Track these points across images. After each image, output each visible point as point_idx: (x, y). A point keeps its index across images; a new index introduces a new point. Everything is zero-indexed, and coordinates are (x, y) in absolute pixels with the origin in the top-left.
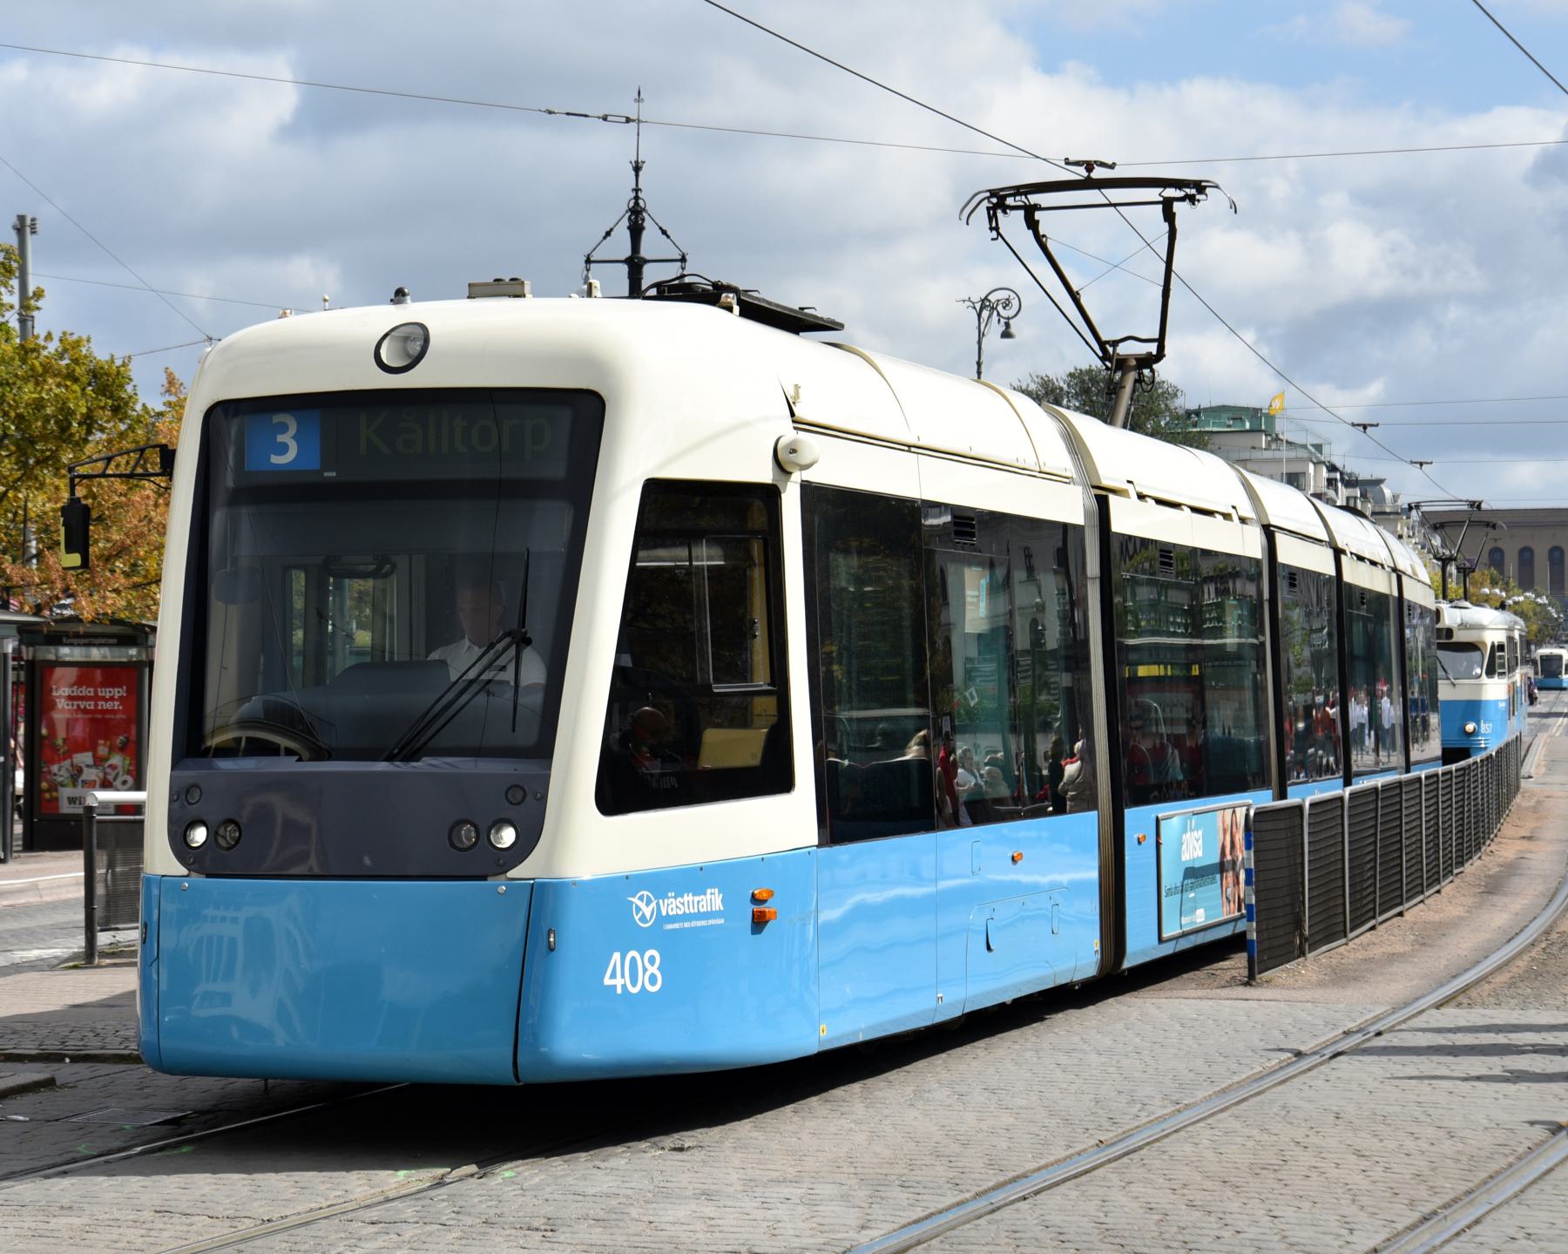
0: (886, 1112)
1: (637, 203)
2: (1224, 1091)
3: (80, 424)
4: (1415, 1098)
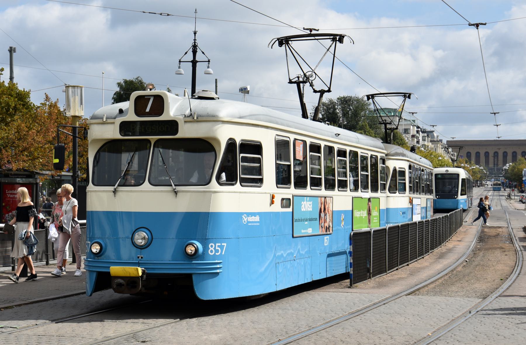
0: (216, 329)
1: (195, 44)
2: (327, 323)
3: (12, 110)
4: (386, 325)
